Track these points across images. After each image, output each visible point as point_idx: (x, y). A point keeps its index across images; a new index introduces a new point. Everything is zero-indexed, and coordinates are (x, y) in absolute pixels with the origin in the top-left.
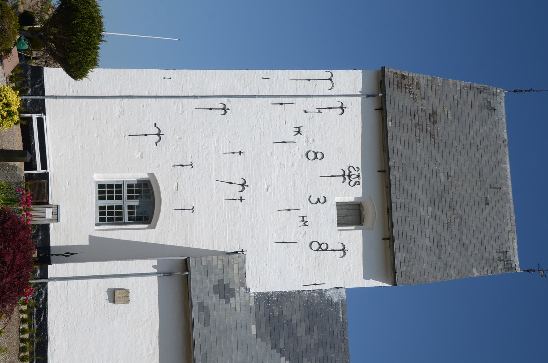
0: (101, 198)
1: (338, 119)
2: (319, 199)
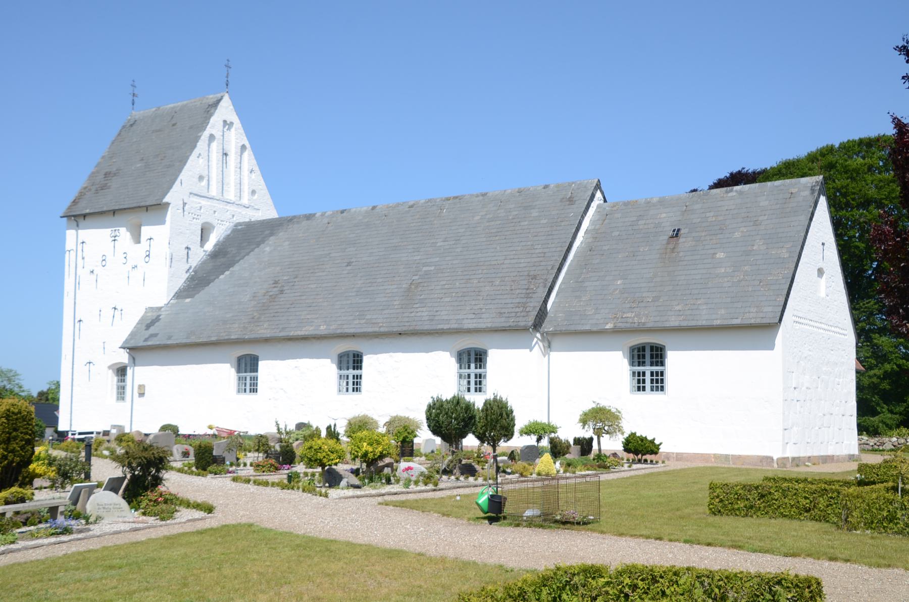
0: (245, 391)
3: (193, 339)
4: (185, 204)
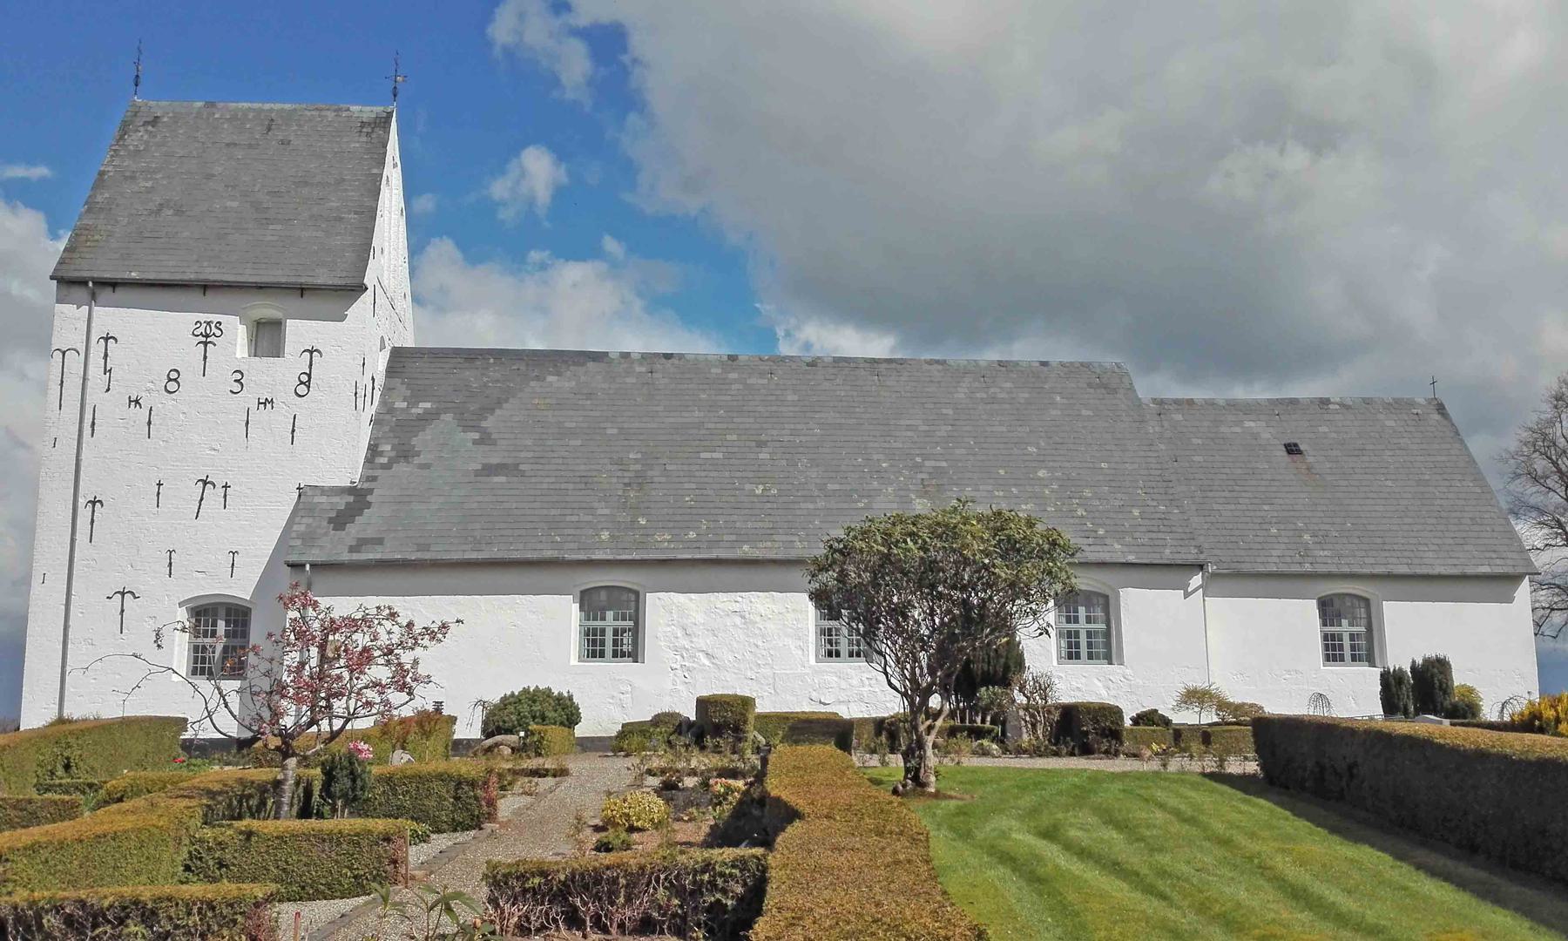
1: (123, 346)
2: (235, 381)
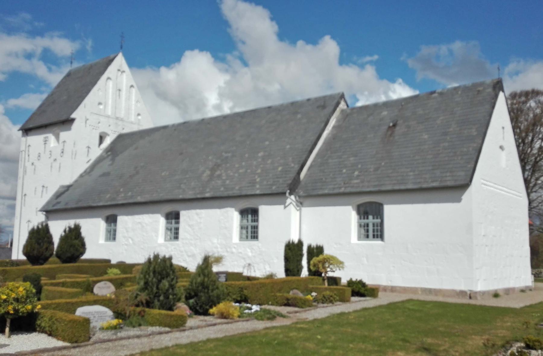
3: (80, 205)
4: (87, 120)
